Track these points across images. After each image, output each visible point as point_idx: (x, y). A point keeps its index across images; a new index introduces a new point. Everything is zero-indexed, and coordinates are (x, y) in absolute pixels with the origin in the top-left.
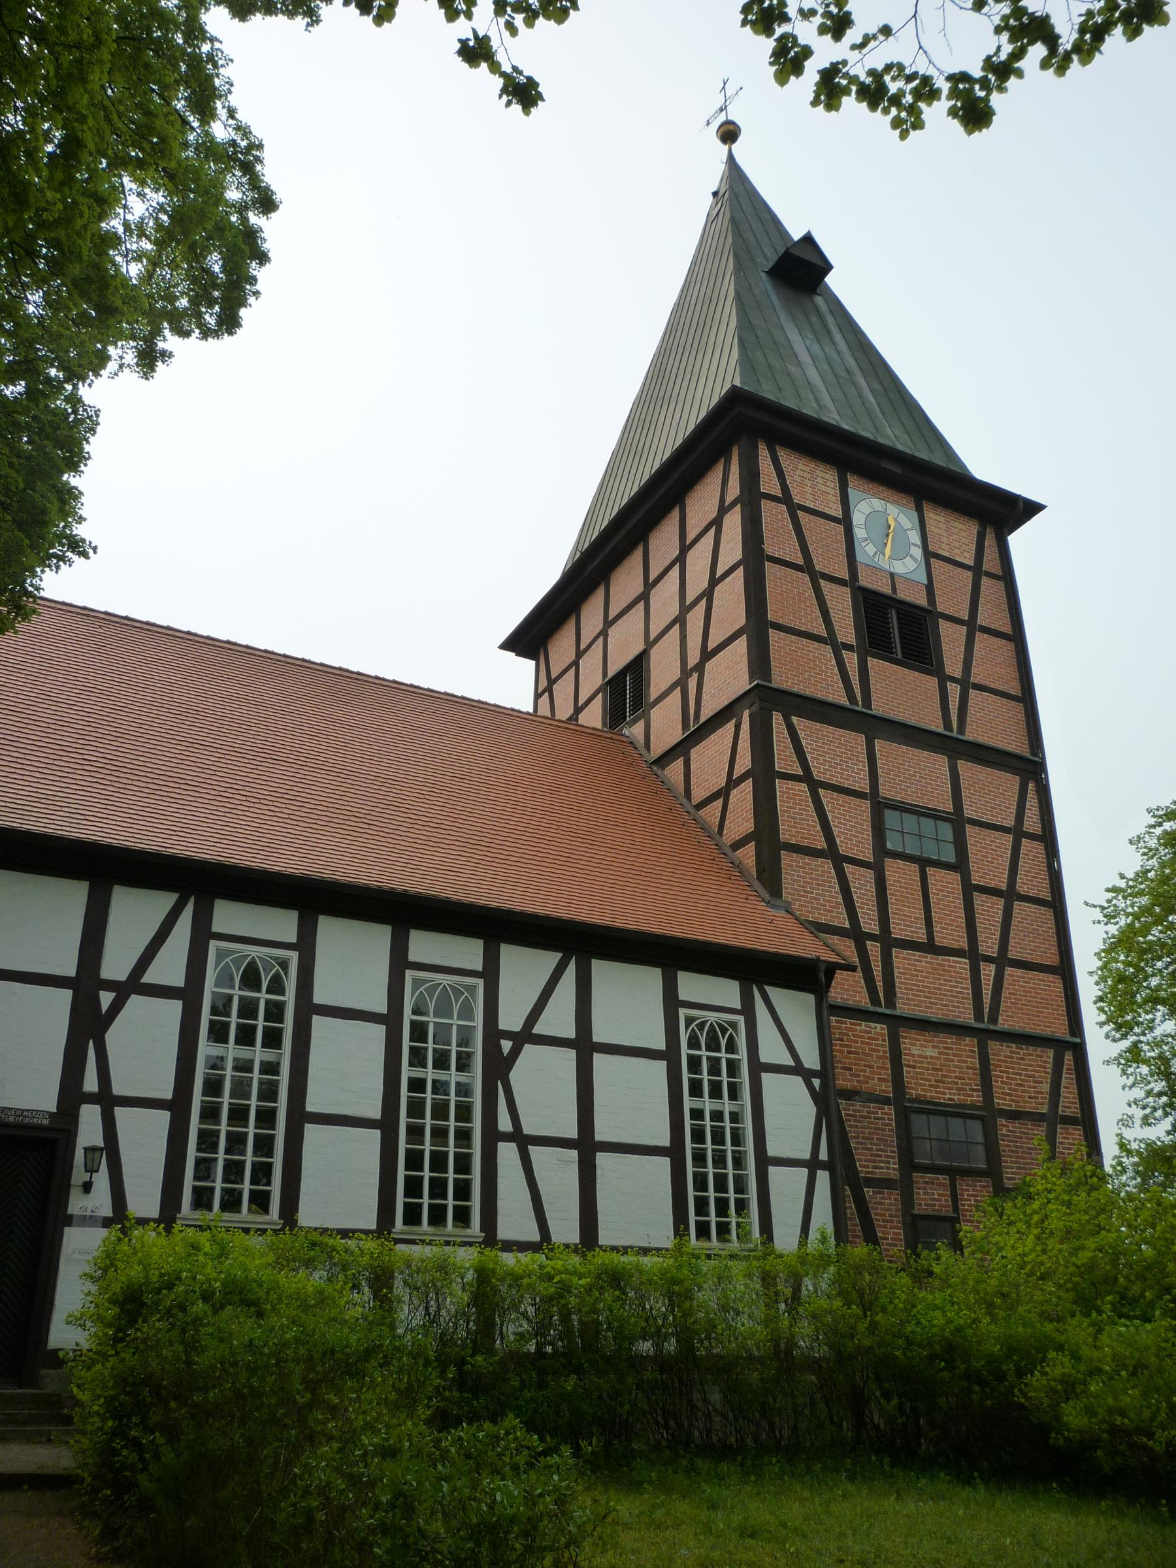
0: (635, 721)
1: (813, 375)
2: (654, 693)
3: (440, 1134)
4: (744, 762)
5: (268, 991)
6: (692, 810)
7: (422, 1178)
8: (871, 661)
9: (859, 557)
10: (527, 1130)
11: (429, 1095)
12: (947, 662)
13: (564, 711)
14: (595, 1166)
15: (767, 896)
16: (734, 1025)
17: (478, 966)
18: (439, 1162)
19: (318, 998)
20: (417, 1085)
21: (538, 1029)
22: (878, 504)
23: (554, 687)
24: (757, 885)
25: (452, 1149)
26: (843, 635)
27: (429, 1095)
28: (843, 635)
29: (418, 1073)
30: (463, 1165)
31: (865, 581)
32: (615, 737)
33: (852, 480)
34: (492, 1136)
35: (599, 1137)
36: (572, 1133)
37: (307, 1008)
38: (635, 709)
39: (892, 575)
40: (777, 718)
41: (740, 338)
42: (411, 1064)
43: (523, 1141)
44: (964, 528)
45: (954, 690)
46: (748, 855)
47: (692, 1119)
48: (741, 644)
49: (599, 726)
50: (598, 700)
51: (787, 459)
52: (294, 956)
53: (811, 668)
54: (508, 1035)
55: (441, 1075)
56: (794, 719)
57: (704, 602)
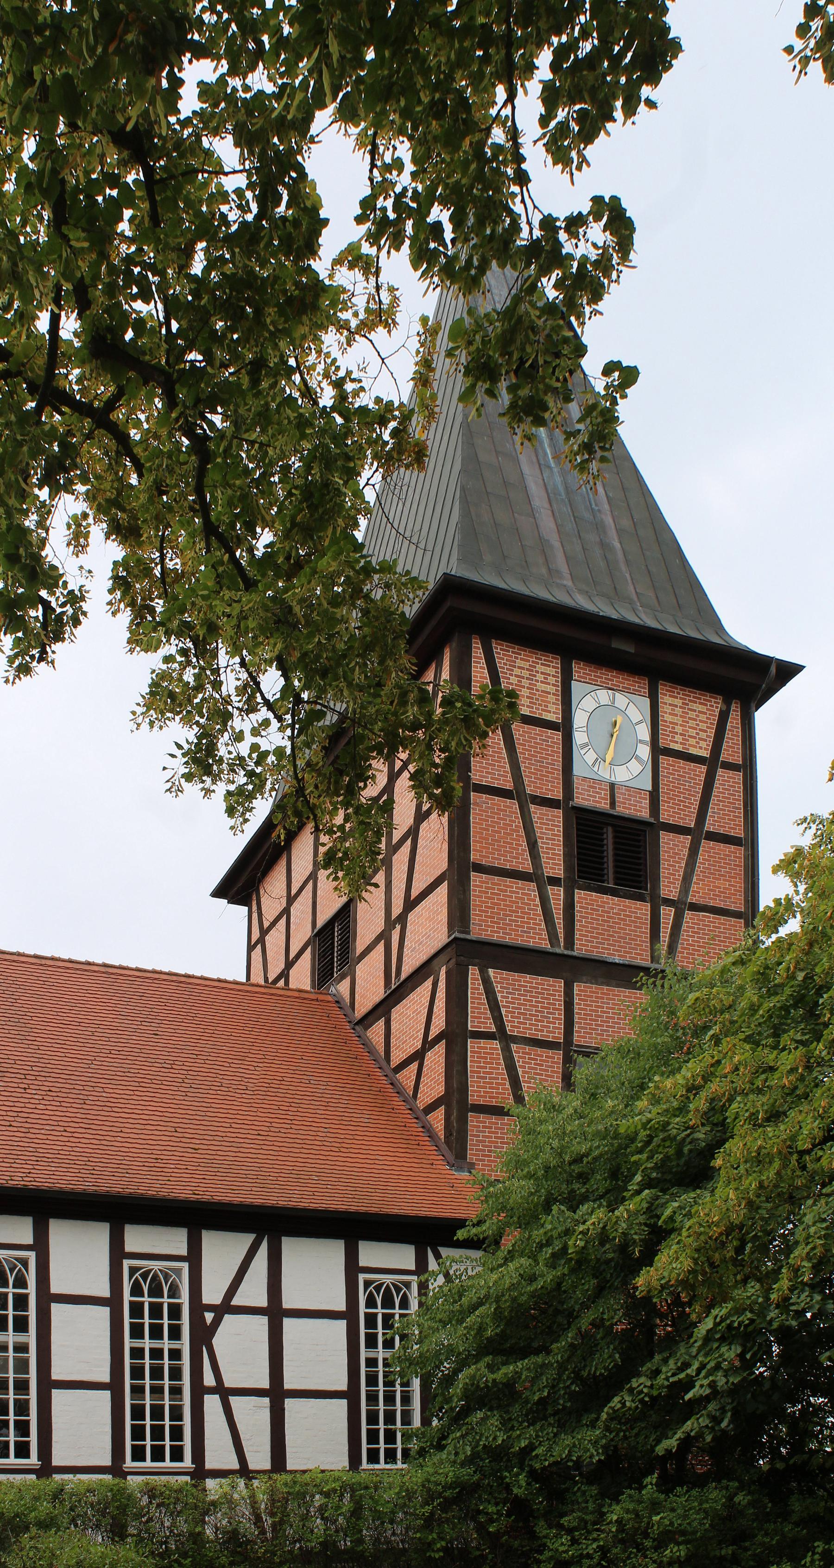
0: (342, 977)
1: (547, 524)
2: (360, 947)
3: (157, 1391)
4: (439, 1023)
5: (14, 1287)
6: (391, 1074)
7: (144, 1426)
8: (579, 894)
9: (578, 770)
10: (229, 1382)
11: (166, 1361)
12: (663, 882)
13: (276, 967)
14: (284, 1409)
15: (451, 1158)
16: (407, 1285)
17: (183, 1251)
18: (157, 1412)
19: (56, 1288)
20: (137, 1353)
21: (236, 1301)
22: (604, 696)
23: (267, 938)
24: (444, 1147)
25: (167, 1402)
26: (551, 868)
27: (166, 1361)
28: (551, 868)
29: (137, 1343)
30: (177, 1414)
31: (583, 798)
32: (321, 997)
33: (578, 669)
34: (199, 1391)
35: (287, 1386)
36: (265, 1384)
37: (46, 1298)
38: (343, 964)
39: (612, 786)
40: (473, 972)
41: (463, 489)
42: (132, 1337)
43: (225, 1393)
44: (703, 708)
45: (667, 914)
46: (438, 1119)
47: (132, 1358)
48: (442, 892)
49: (308, 988)
50: (307, 954)
51: (502, 653)
52: (32, 1256)
53: (514, 911)
54: (210, 1308)
55: (156, 1344)
56: (491, 972)
57: (409, 842)
